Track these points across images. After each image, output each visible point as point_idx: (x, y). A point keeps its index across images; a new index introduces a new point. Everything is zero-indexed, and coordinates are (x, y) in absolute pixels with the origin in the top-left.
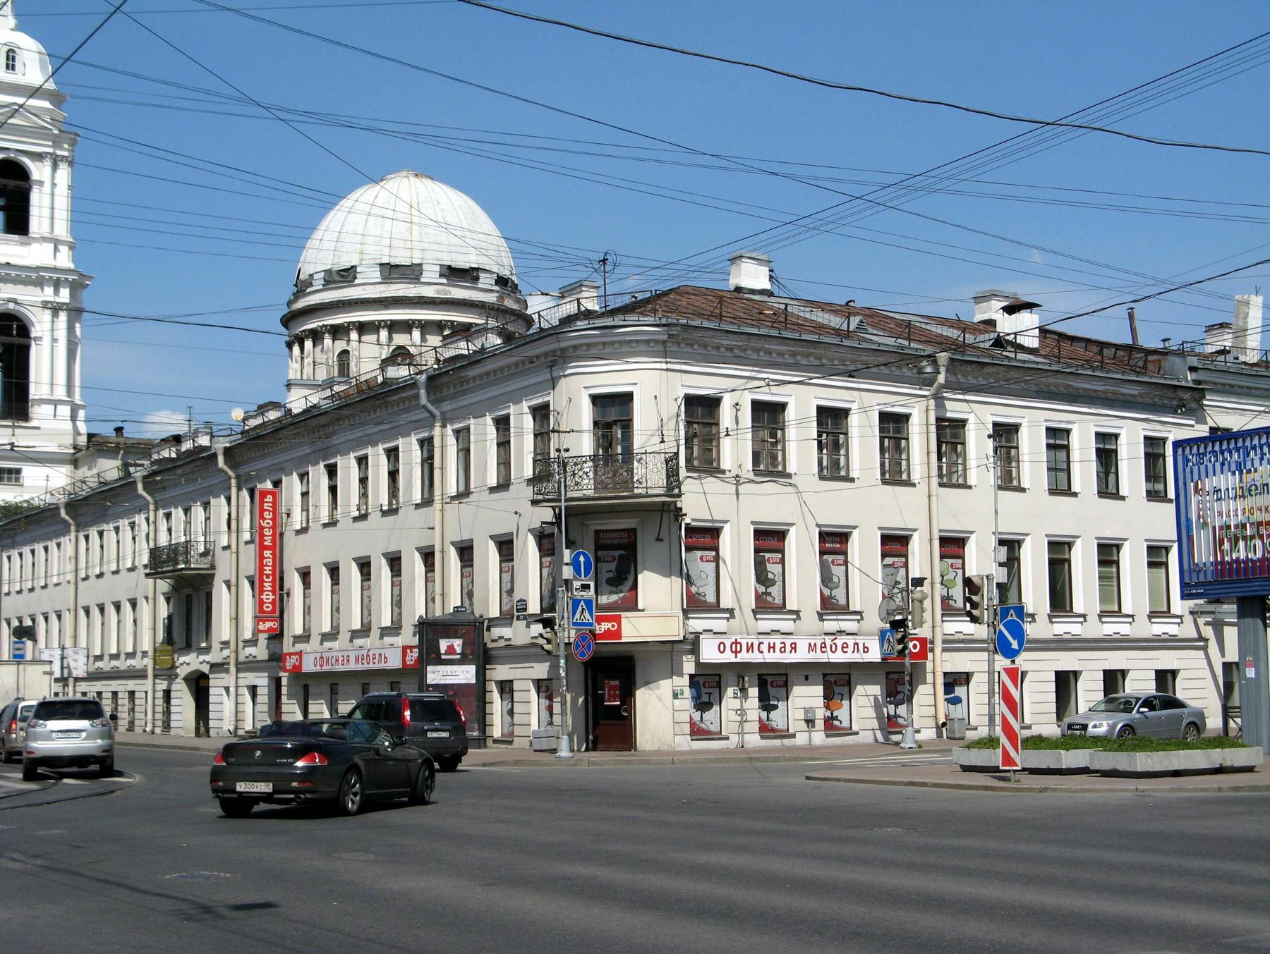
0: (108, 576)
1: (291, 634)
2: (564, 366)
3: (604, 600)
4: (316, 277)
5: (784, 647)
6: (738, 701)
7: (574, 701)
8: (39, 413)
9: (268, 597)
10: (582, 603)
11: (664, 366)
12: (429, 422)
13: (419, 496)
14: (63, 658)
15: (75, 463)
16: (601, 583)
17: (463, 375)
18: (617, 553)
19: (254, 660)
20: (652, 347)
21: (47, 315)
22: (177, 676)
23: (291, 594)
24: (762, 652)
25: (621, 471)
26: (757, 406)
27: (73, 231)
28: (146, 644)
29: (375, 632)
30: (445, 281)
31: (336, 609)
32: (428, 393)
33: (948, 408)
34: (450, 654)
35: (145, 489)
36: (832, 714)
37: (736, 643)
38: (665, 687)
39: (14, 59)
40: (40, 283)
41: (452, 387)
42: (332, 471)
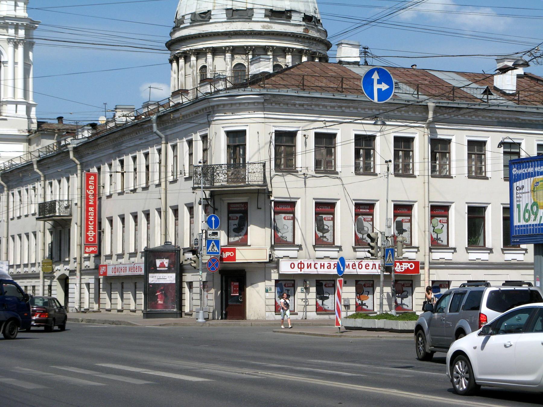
1: (104, 255)
2: (213, 115)
3: (232, 240)
4: (186, 17)
5: (330, 266)
6: (304, 294)
9: (91, 233)
10: (213, 242)
11: (263, 116)
15: (29, 141)
16: (230, 231)
18: (238, 215)
20: (256, 106)
21: (10, 48)
22: (54, 277)
24: (317, 268)
26: (318, 136)
28: (40, 260)
30: (268, 20)
32: (158, 126)
33: (438, 133)
36: (362, 302)
37: (301, 263)
38: (261, 286)
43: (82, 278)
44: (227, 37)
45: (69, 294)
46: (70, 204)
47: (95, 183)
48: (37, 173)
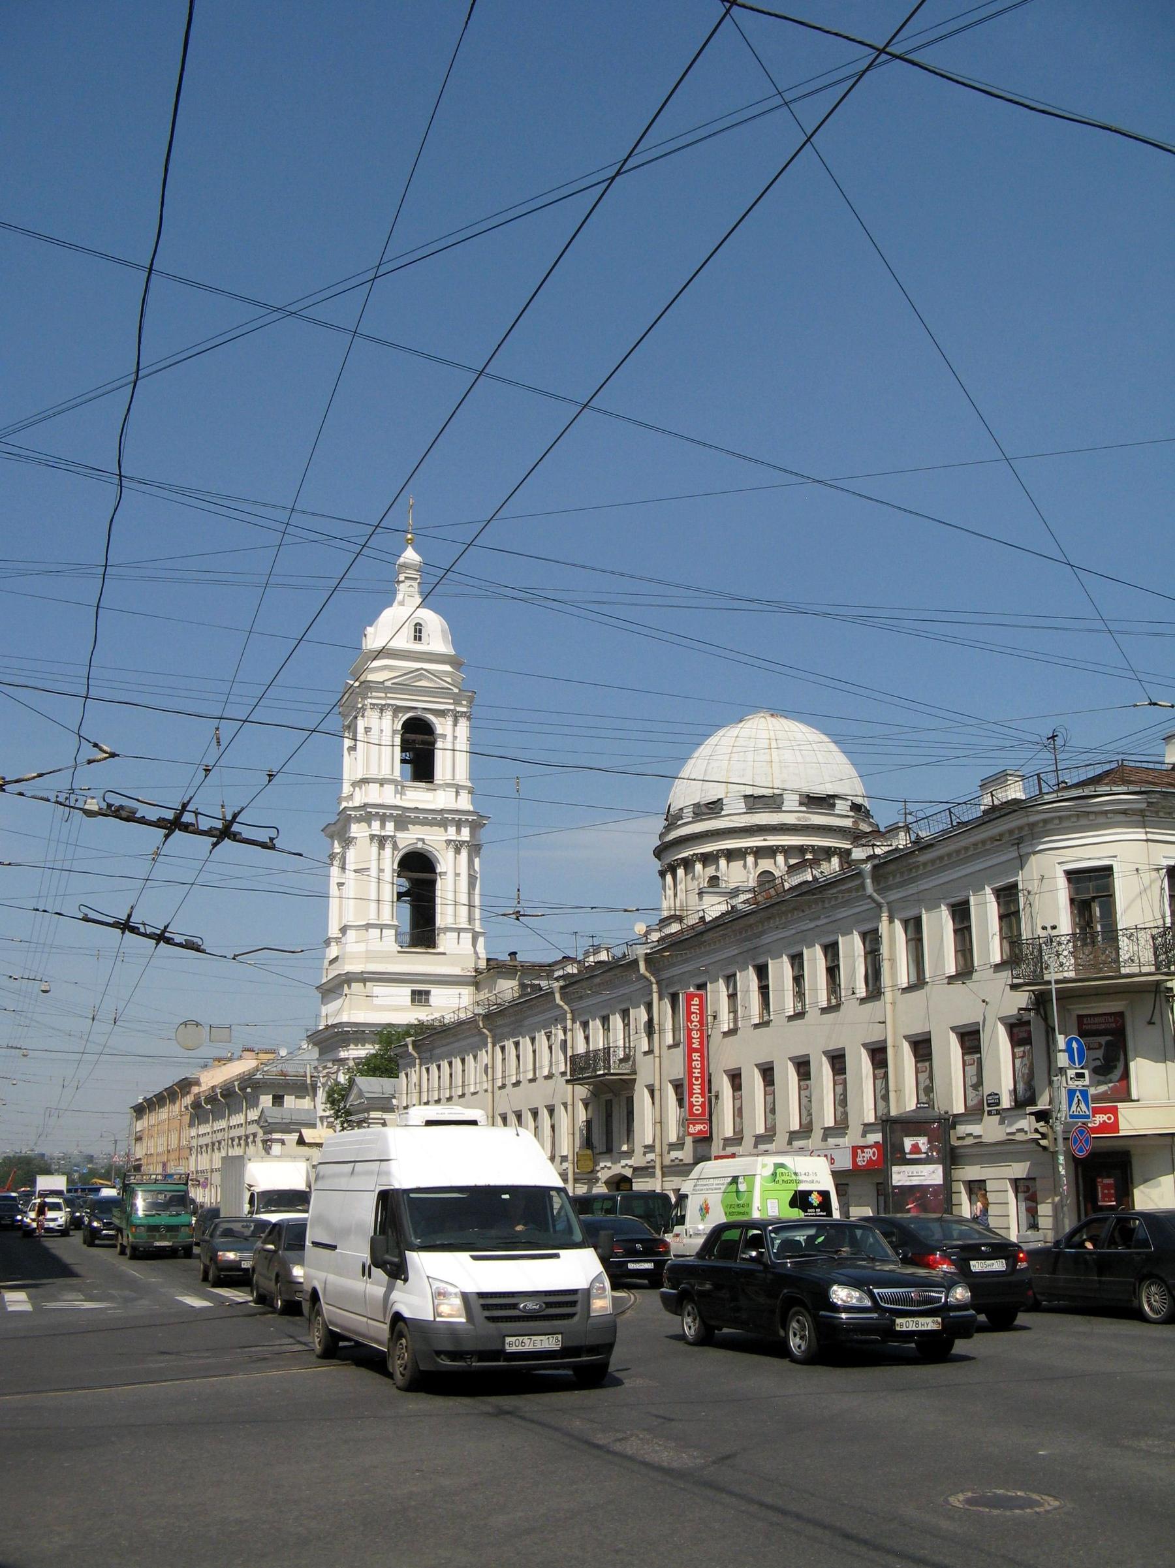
0: (524, 1084)
8: (446, 942)
10: (1078, 1094)
11: (1143, 837)
15: (477, 985)
18: (1103, 1040)
19: (681, 1163)
21: (451, 853)
22: (597, 1180)
29: (817, 1133)
30: (804, 809)
31: (771, 1110)
34: (915, 1154)
39: (420, 630)
40: (444, 824)
41: (898, 875)
47: (701, 1009)
48: (561, 1007)
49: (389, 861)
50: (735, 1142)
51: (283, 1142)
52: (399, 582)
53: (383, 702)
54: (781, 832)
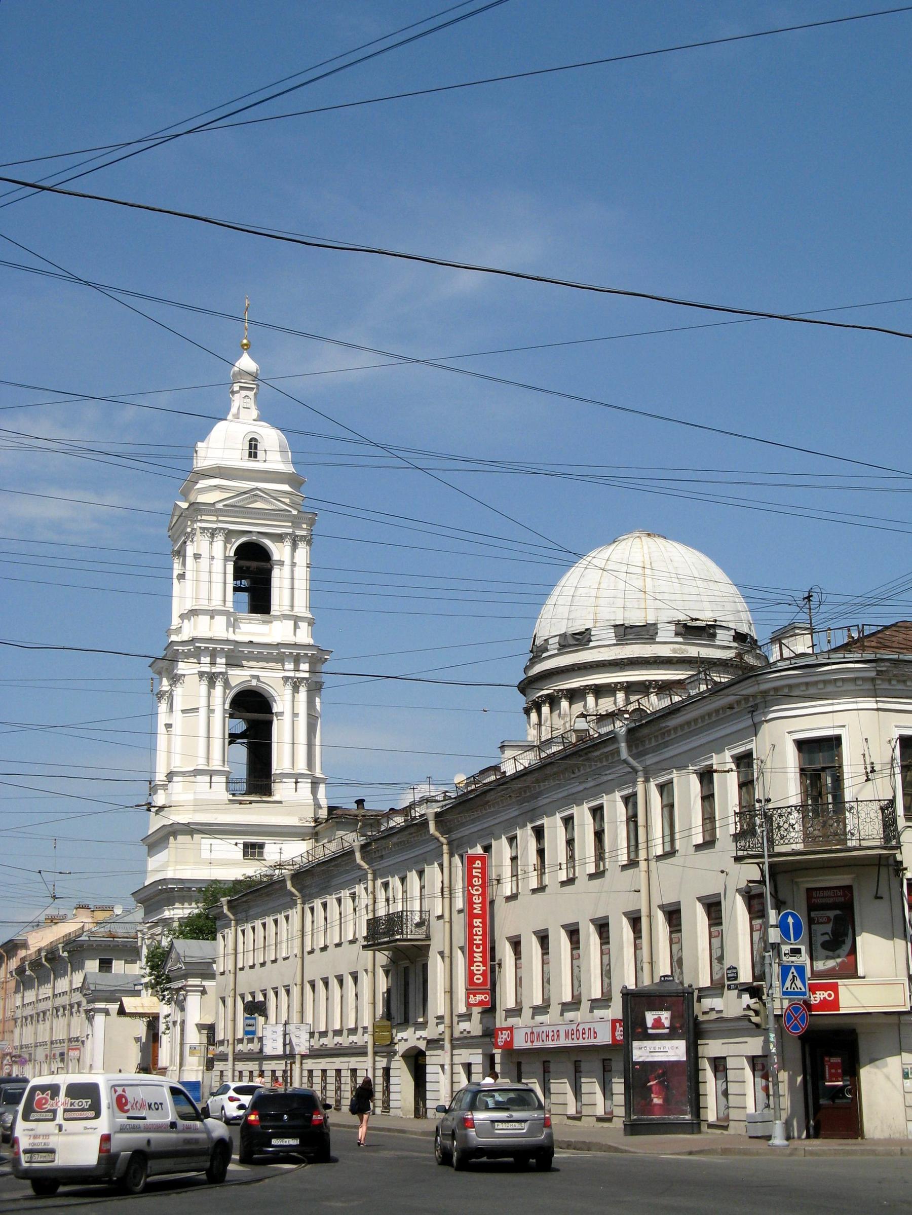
2: (766, 710)
3: (820, 966)
4: (551, 641)
7: (792, 1080)
8: (282, 790)
10: (793, 970)
11: (874, 706)
12: (630, 777)
13: (625, 857)
14: (285, 1035)
15: (315, 835)
17: (664, 725)
18: (831, 914)
19: (469, 1035)
20: (859, 685)
21: (288, 690)
22: (395, 1053)
23: (503, 965)
25: (831, 822)
27: (311, 607)
28: (367, 1021)
29: (585, 1005)
30: (680, 639)
31: (546, 981)
32: (629, 747)
35: (363, 858)
39: (256, 446)
40: (280, 659)
41: (653, 740)
42: (539, 833)
43: (454, 1053)
44: (617, 668)
45: (427, 1084)
46: (427, 918)
49: (220, 699)
50: (514, 1013)
51: (107, 1012)
52: (233, 393)
53: (214, 526)
54: (655, 666)
